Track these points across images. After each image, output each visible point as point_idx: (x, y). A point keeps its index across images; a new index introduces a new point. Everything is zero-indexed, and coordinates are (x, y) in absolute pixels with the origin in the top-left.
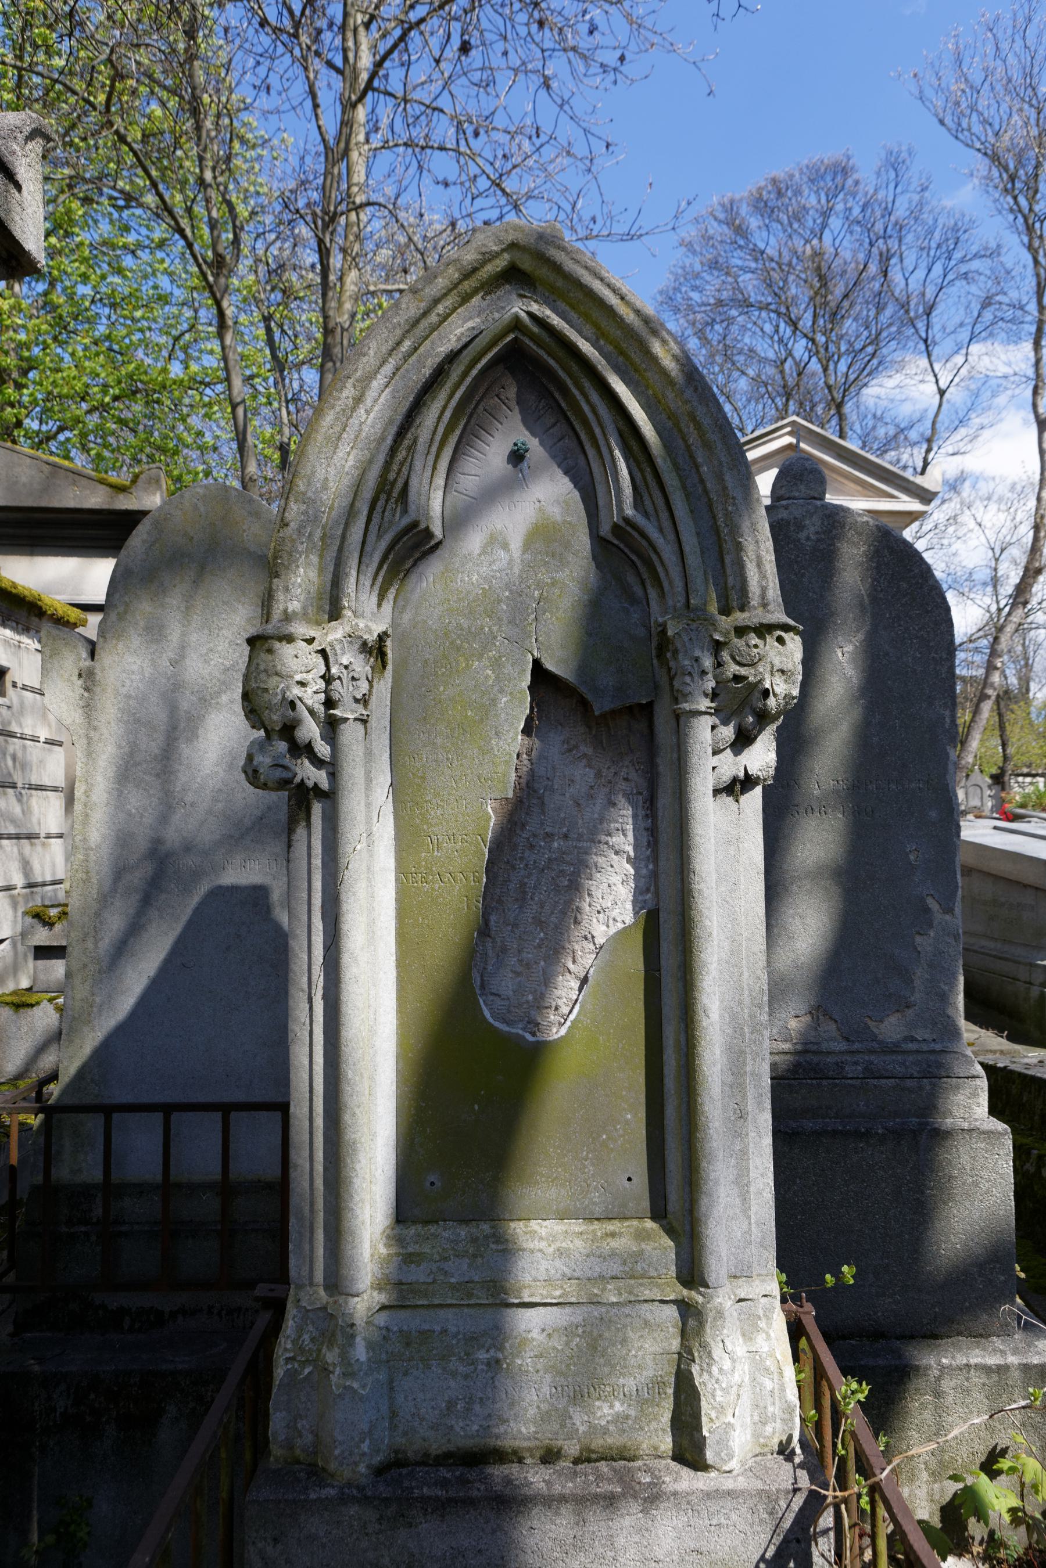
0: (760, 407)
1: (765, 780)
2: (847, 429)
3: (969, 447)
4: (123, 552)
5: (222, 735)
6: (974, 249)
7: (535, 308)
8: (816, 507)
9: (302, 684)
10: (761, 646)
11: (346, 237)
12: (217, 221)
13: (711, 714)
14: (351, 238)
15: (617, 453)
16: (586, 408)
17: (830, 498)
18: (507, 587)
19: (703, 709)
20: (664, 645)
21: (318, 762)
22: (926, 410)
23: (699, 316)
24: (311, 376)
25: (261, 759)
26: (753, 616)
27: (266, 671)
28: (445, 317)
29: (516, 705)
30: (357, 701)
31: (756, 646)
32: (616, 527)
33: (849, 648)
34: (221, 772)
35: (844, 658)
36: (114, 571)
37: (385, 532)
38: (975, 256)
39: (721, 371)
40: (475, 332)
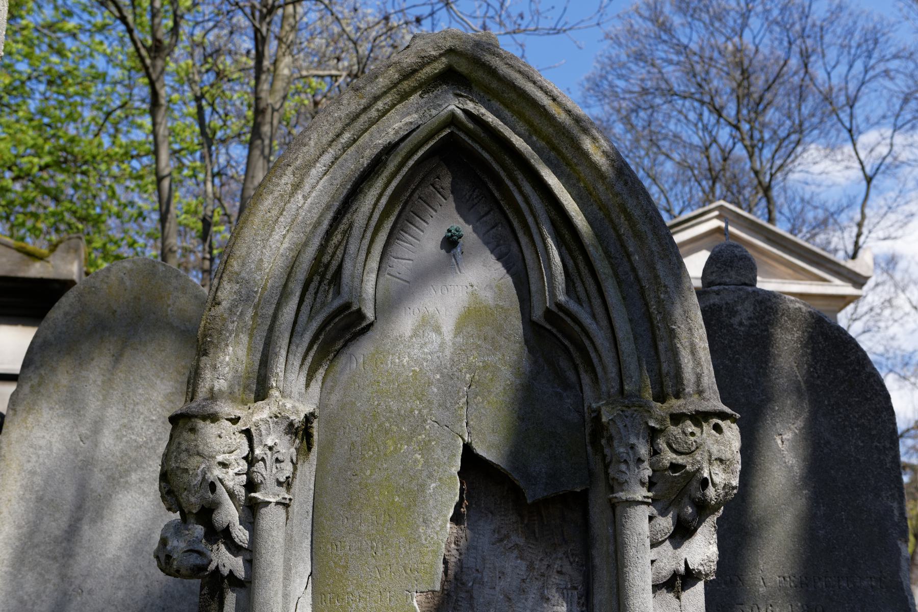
0: (687, 189)
1: (707, 575)
2: (776, 214)
3: (900, 233)
4: (44, 324)
5: (135, 514)
6: (893, 50)
7: (470, 106)
8: (748, 293)
9: (224, 465)
10: (698, 434)
11: (282, 27)
12: (159, 11)
13: (648, 504)
14: (287, 28)
15: (550, 241)
16: (519, 199)
17: (765, 284)
18: (439, 370)
19: (640, 499)
20: (598, 432)
21: (235, 548)
22: (855, 197)
23: (624, 104)
24: (238, 152)
25: (175, 543)
26: (690, 404)
27: (187, 450)
28: (384, 113)
29: (447, 491)
30: (280, 484)
31: (693, 434)
32: (548, 313)
33: (788, 436)
34: (124, 556)
35: (785, 444)
36: (32, 343)
37: (317, 313)
38: (896, 57)
39: (647, 154)
40: (413, 127)
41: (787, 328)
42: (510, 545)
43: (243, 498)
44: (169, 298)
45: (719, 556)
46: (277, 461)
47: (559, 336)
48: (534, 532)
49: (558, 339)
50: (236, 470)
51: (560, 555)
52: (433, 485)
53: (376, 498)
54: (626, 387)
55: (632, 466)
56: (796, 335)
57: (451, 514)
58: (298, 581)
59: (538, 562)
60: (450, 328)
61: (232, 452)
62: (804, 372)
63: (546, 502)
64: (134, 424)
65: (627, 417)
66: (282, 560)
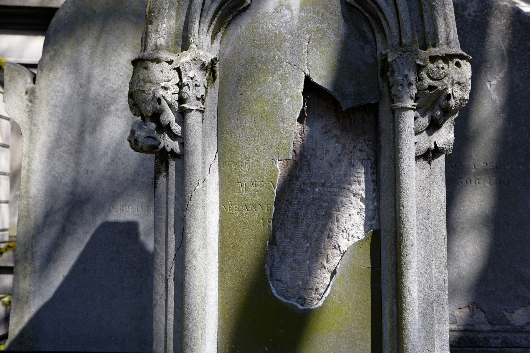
1: (447, 151)
9: (165, 88)
18: (290, 32)
19: (410, 106)
20: (386, 67)
21: (174, 136)
25: (139, 133)
26: (442, 50)
27: (143, 80)
29: (294, 102)
30: (198, 99)
31: (443, 68)
33: (494, 82)
41: (498, 18)
42: (332, 135)
43: (177, 108)
44: (126, 3)
45: (455, 140)
46: (196, 85)
47: (363, 11)
48: (346, 128)
49: (362, 13)
50: (172, 91)
51: (361, 141)
52: (287, 100)
53: (254, 107)
54: (403, 41)
55: (405, 88)
56: (503, 22)
57: (298, 116)
58: (210, 155)
59: (348, 145)
60: (296, 7)
61: (169, 81)
62: (506, 44)
63: (353, 110)
64: (110, 78)
65: (403, 58)
66: (201, 143)
